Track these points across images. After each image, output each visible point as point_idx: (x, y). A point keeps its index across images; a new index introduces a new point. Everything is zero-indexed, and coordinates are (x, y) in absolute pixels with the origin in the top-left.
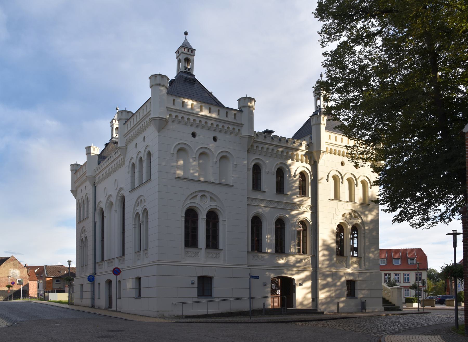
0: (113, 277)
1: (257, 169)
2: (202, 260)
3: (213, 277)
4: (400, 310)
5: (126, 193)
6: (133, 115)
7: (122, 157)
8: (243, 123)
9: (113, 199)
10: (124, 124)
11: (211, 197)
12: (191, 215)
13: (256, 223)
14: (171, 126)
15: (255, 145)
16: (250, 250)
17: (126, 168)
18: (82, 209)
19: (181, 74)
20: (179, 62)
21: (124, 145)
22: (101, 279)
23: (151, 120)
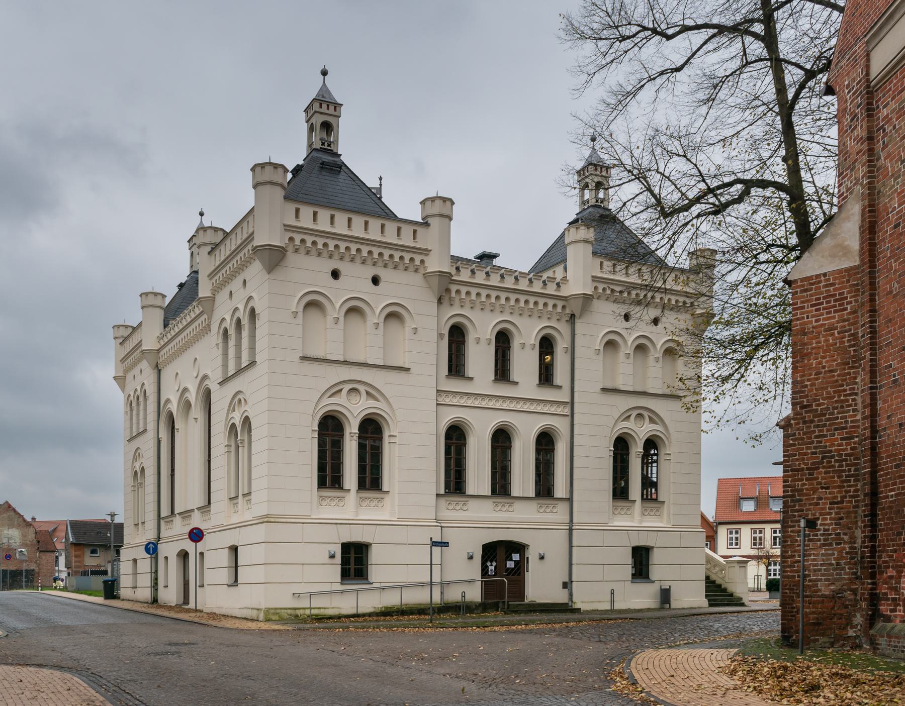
0: (189, 546)
1: (457, 336)
2: (352, 513)
3: (371, 544)
4: (743, 605)
5: (213, 386)
6: (227, 235)
7: (205, 316)
8: (429, 248)
9: (192, 396)
10: (209, 253)
11: (368, 393)
12: (330, 427)
13: (456, 436)
14: (292, 258)
15: (454, 288)
16: (442, 492)
17: (214, 337)
18: (134, 412)
19: (315, 154)
20: (311, 129)
21: (210, 295)
22: (169, 550)
23: (256, 249)
